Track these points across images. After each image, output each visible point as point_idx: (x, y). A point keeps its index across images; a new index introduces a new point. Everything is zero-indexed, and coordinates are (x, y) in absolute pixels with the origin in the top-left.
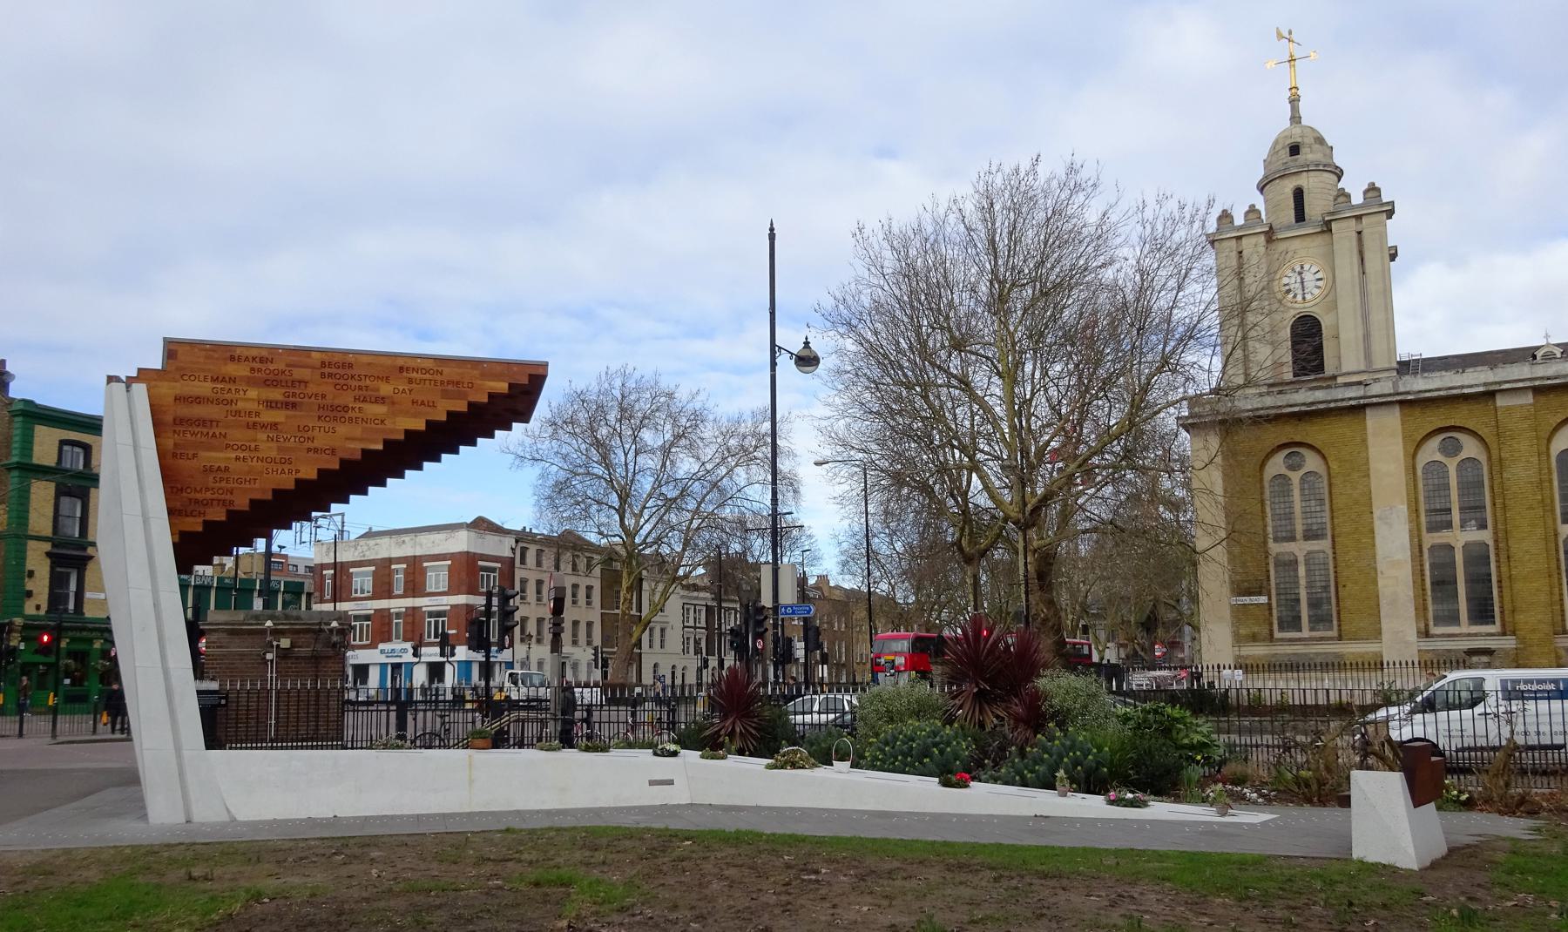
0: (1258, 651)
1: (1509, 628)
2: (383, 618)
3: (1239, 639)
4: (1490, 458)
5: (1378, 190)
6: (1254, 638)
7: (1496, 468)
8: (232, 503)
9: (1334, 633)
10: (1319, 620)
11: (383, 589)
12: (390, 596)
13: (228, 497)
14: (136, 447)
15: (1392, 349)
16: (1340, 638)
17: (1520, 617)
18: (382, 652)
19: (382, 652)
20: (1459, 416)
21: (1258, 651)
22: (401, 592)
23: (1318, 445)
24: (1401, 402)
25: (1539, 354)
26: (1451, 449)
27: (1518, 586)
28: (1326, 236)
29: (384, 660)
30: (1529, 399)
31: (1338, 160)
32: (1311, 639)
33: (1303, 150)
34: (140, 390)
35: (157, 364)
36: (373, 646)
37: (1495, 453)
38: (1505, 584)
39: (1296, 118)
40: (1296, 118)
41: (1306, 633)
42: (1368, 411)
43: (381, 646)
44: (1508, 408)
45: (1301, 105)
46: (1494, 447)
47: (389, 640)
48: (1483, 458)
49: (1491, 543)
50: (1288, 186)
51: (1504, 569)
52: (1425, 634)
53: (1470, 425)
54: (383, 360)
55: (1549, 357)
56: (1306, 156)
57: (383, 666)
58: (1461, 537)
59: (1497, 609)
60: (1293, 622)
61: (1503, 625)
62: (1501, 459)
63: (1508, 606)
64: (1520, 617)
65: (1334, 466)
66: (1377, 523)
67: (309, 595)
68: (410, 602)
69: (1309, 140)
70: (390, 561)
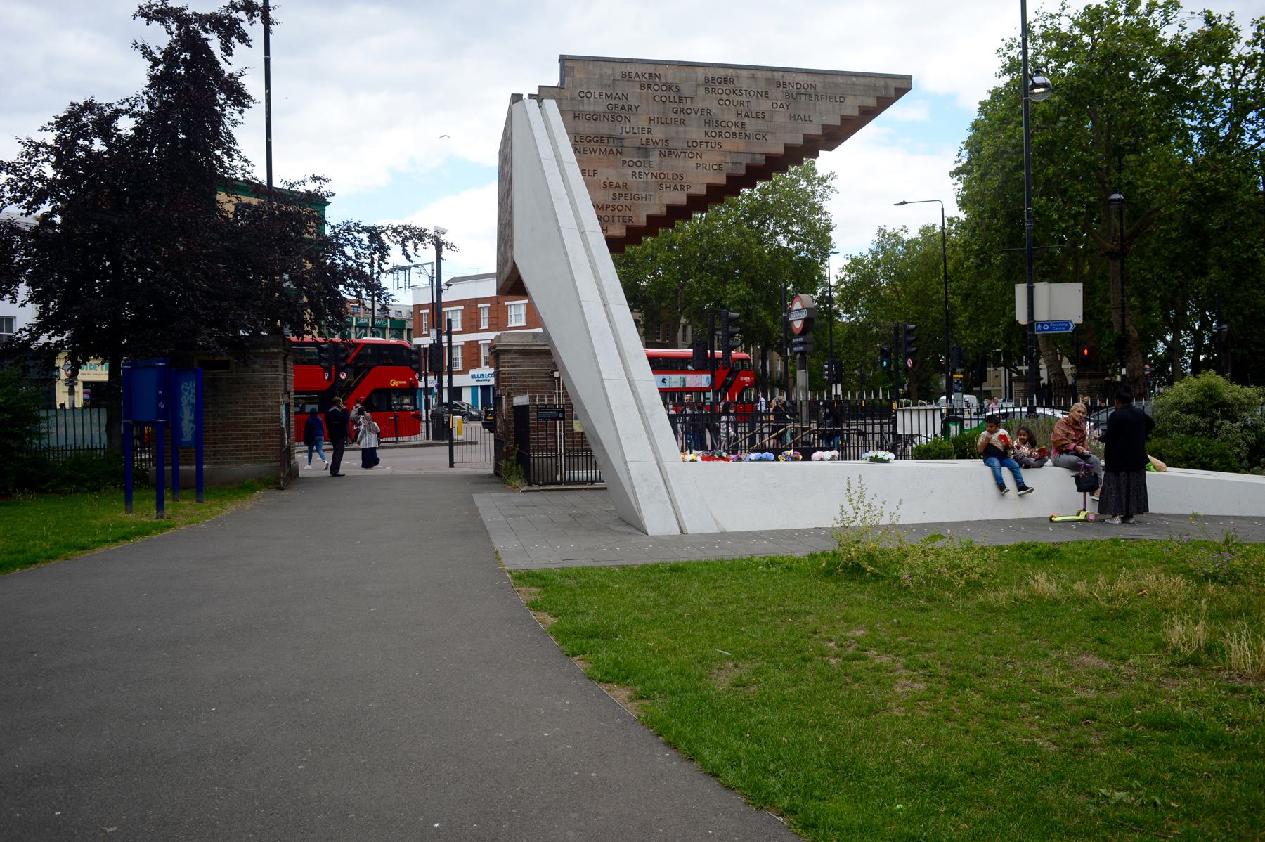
2: (472, 347)
8: (631, 218)
11: (471, 324)
12: (477, 329)
13: (627, 213)
14: (559, 162)
18: (473, 376)
19: (473, 376)
22: (460, 329)
29: (474, 383)
34: (551, 105)
35: (554, 80)
36: (465, 371)
43: (472, 372)
47: (479, 366)
54: (800, 78)
57: (474, 388)
67: (409, 330)
68: (493, 335)
70: (478, 301)
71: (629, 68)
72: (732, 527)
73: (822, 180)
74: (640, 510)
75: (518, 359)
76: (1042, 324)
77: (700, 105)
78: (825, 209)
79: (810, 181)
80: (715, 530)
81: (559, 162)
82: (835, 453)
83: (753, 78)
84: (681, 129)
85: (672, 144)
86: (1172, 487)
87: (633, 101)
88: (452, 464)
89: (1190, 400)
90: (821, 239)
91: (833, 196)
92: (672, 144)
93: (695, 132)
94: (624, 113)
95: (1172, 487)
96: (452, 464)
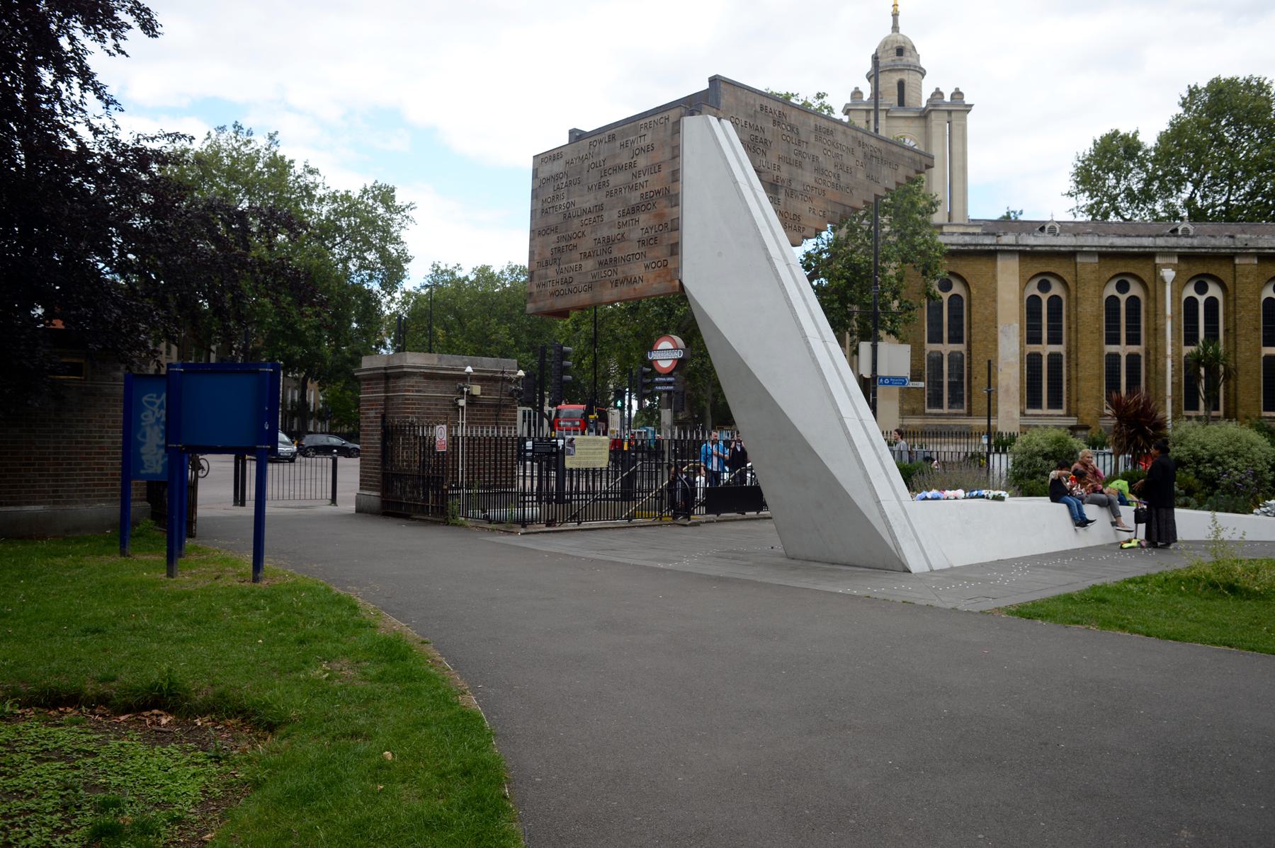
0: (915, 422)
1: (1073, 411)
3: (903, 414)
4: (1068, 296)
5: (961, 94)
6: (913, 413)
7: (1073, 304)
9: (965, 411)
10: (956, 400)
14: (752, 189)
15: (965, 211)
16: (969, 414)
17: (1081, 405)
20: (1213, 269)
21: (915, 422)
23: (964, 275)
24: (1020, 252)
25: (1047, 227)
26: (1201, 289)
27: (1082, 384)
28: (922, 123)
30: (1096, 259)
31: (923, 64)
32: (949, 414)
33: (907, 54)
37: (1073, 293)
38: (1074, 382)
39: (895, 28)
40: (895, 28)
41: (946, 410)
42: (999, 257)
44: (1083, 264)
45: (900, 18)
46: (1073, 288)
48: (1063, 296)
49: (1142, 354)
50: (896, 77)
51: (1073, 372)
52: (1023, 414)
53: (1060, 273)
55: (1052, 231)
56: (907, 59)
58: (1046, 349)
59: (1064, 399)
60: (936, 401)
61: (1069, 409)
62: (1076, 298)
63: (1074, 398)
64: (1081, 405)
65: (974, 291)
66: (1000, 335)
69: (908, 47)
71: (765, 102)
72: (956, 565)
73: (399, 210)
74: (898, 548)
75: (423, 383)
76: (884, 378)
77: (812, 151)
78: (403, 239)
79: (388, 208)
80: (947, 566)
81: (752, 189)
82: (960, 493)
83: (844, 133)
84: (800, 171)
85: (794, 186)
86: (1191, 523)
87: (768, 136)
88: (334, 500)
89: (1048, 449)
90: (393, 270)
91: (410, 226)
92: (794, 186)
93: (808, 177)
94: (761, 146)
95: (1191, 523)
96: (334, 500)
